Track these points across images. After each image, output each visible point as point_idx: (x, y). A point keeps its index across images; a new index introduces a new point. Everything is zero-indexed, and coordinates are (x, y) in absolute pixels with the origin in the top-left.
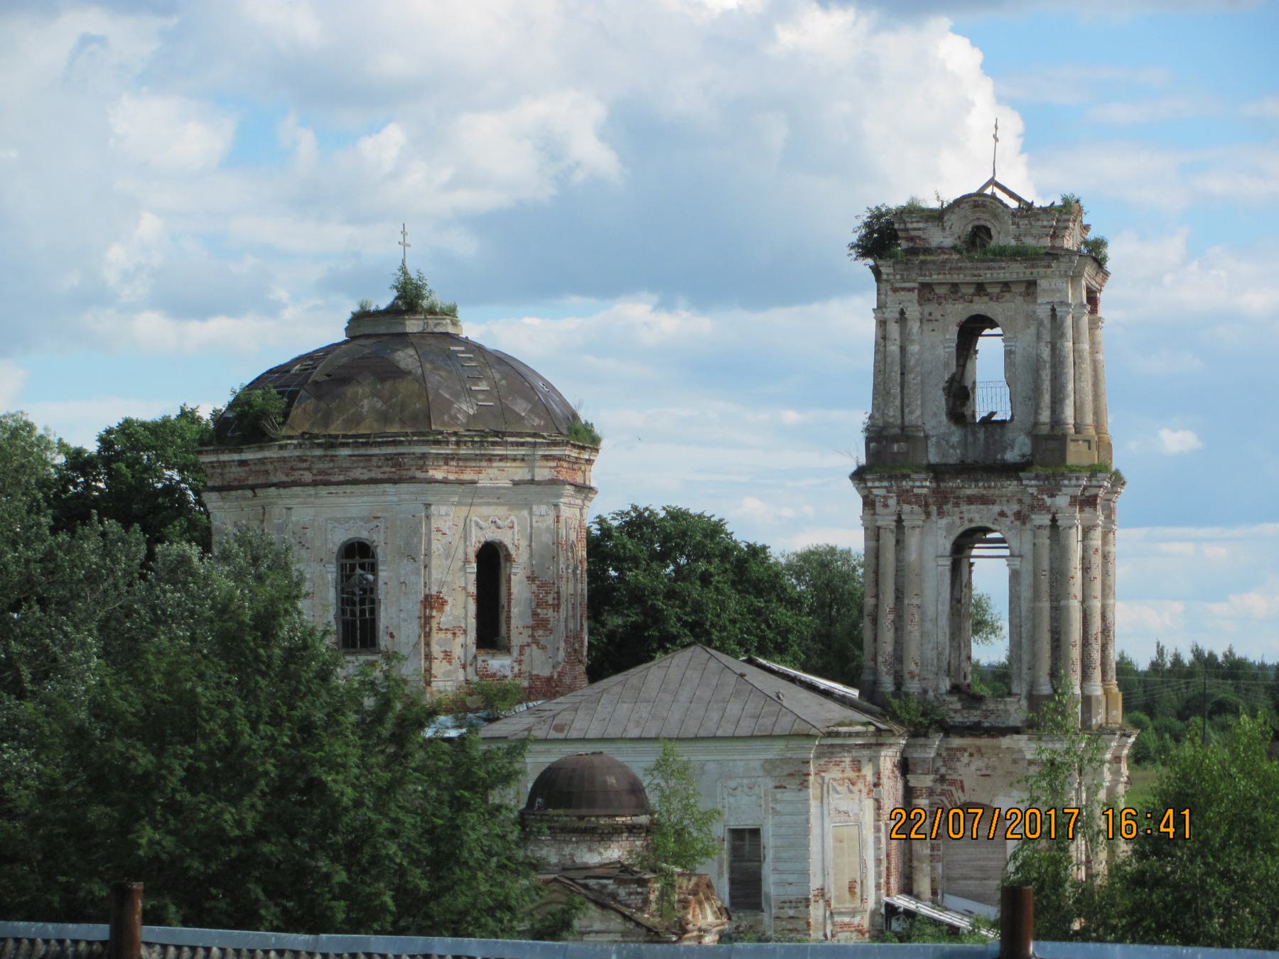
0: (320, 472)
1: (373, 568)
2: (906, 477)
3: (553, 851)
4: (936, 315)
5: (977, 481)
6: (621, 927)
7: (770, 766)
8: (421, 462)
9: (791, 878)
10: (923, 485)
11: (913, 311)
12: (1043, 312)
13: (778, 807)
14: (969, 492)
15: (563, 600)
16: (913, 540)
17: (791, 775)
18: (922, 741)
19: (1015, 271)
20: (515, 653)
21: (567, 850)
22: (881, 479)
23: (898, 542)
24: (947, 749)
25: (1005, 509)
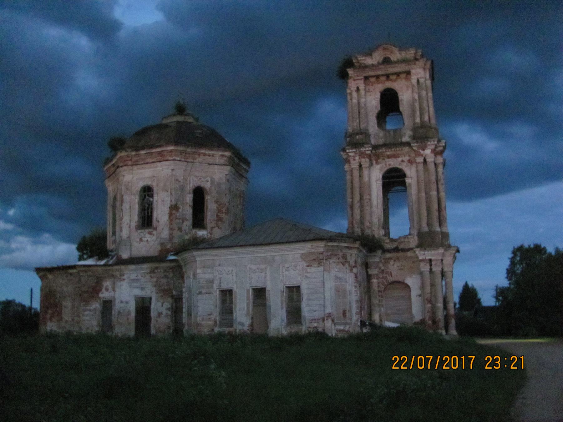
1: (152, 196)
7: (304, 257)
8: (170, 154)
9: (315, 309)
11: (362, 87)
13: (308, 275)
14: (388, 153)
16: (366, 173)
17: (314, 260)
18: (374, 254)
23: (360, 176)
24: (384, 259)
25: (404, 159)
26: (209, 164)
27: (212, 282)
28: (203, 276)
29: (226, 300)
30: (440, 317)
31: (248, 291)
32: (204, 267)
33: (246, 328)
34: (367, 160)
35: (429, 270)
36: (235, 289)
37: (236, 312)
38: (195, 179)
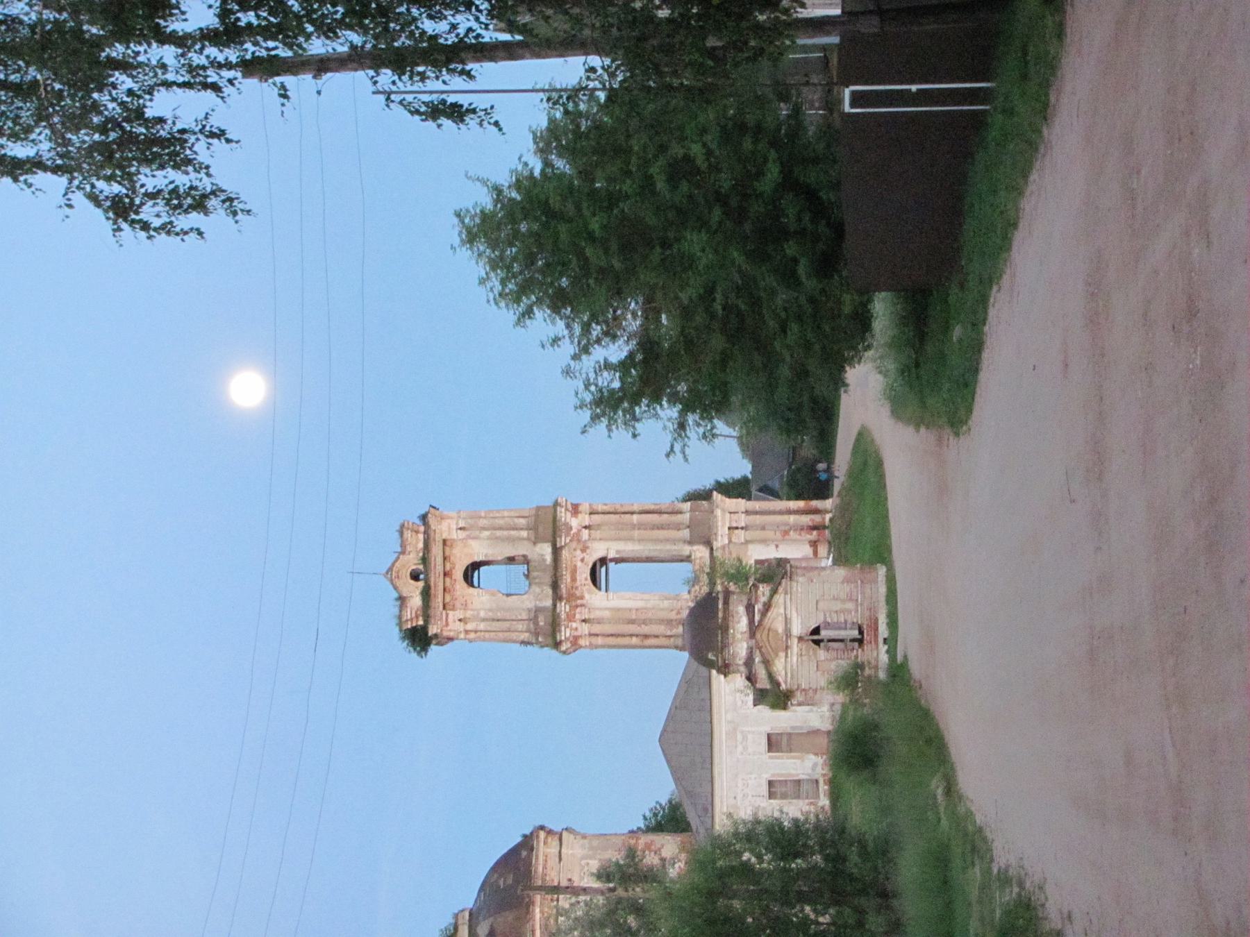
4: (463, 601)
11: (459, 614)
12: (462, 534)
16: (596, 614)
19: (436, 551)
21: (739, 636)
26: (560, 859)
31: (771, 758)
33: (820, 760)
34: (578, 610)
36: (767, 776)
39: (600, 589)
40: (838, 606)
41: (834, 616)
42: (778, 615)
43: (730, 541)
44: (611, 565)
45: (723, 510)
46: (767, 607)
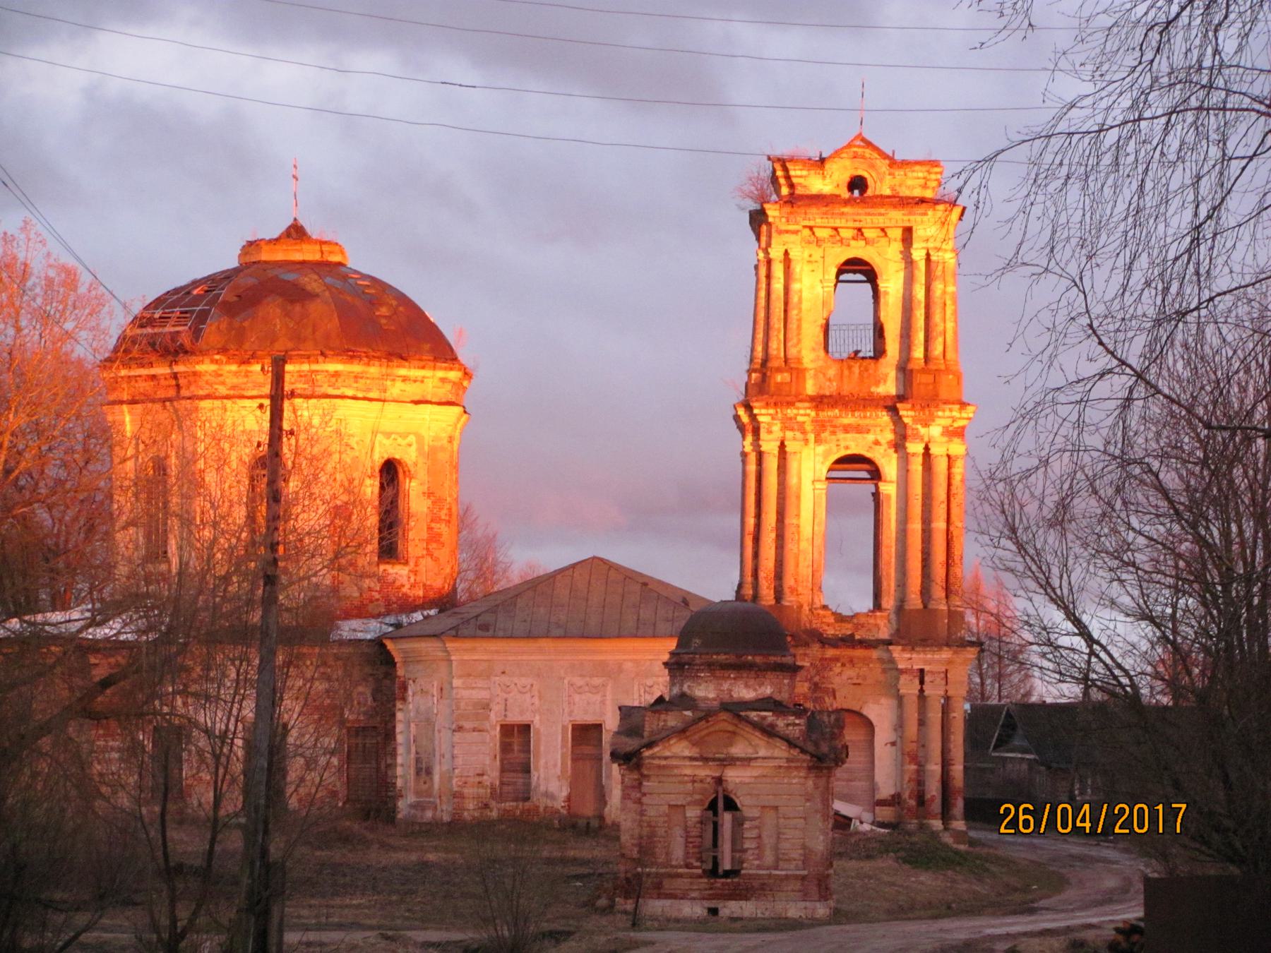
0: (233, 388)
2: (790, 404)
3: (712, 687)
5: (853, 411)
6: (785, 755)
10: (804, 414)
15: (454, 517)
20: (412, 563)
21: (726, 686)
22: (767, 405)
25: (879, 438)
26: (417, 402)
27: (486, 706)
28: (466, 693)
29: (510, 744)
30: (934, 793)
31: (564, 728)
32: (469, 675)
33: (559, 804)
35: (917, 692)
36: (537, 722)
37: (537, 769)
38: (385, 441)
39: (830, 470)
40: (768, 841)
41: (754, 833)
42: (755, 747)
43: (902, 672)
44: (870, 487)
45: (950, 662)
46: (769, 732)
